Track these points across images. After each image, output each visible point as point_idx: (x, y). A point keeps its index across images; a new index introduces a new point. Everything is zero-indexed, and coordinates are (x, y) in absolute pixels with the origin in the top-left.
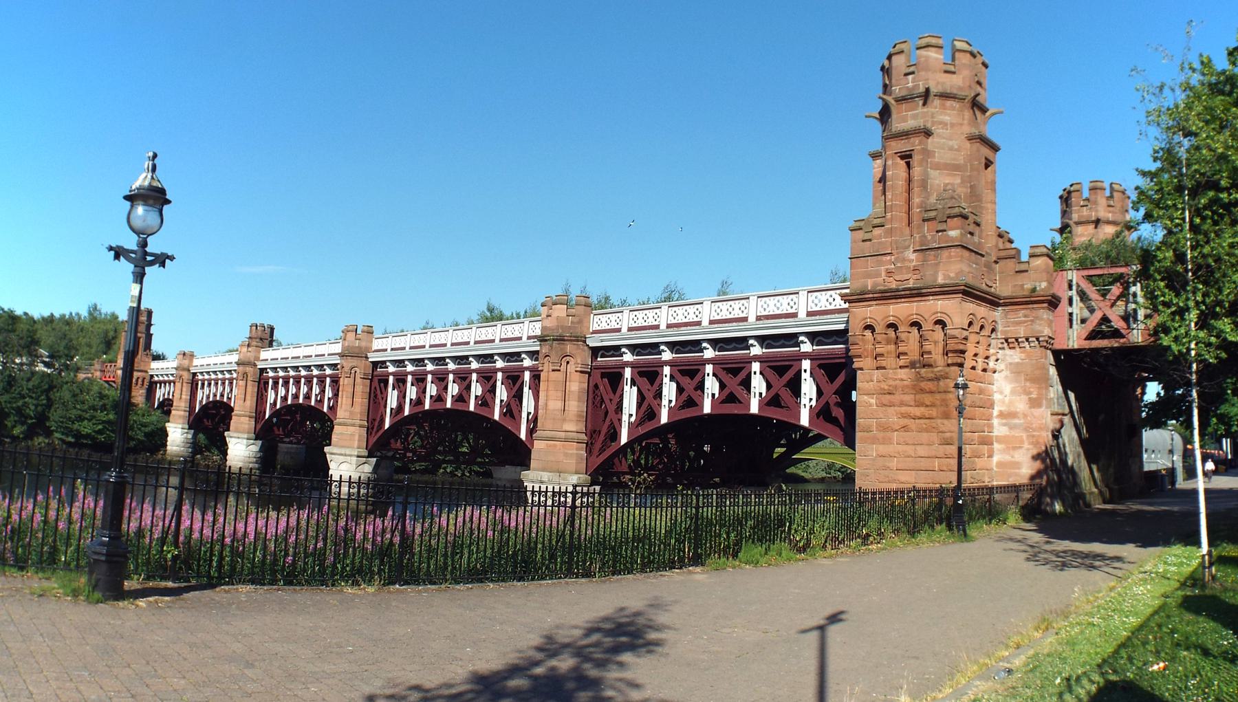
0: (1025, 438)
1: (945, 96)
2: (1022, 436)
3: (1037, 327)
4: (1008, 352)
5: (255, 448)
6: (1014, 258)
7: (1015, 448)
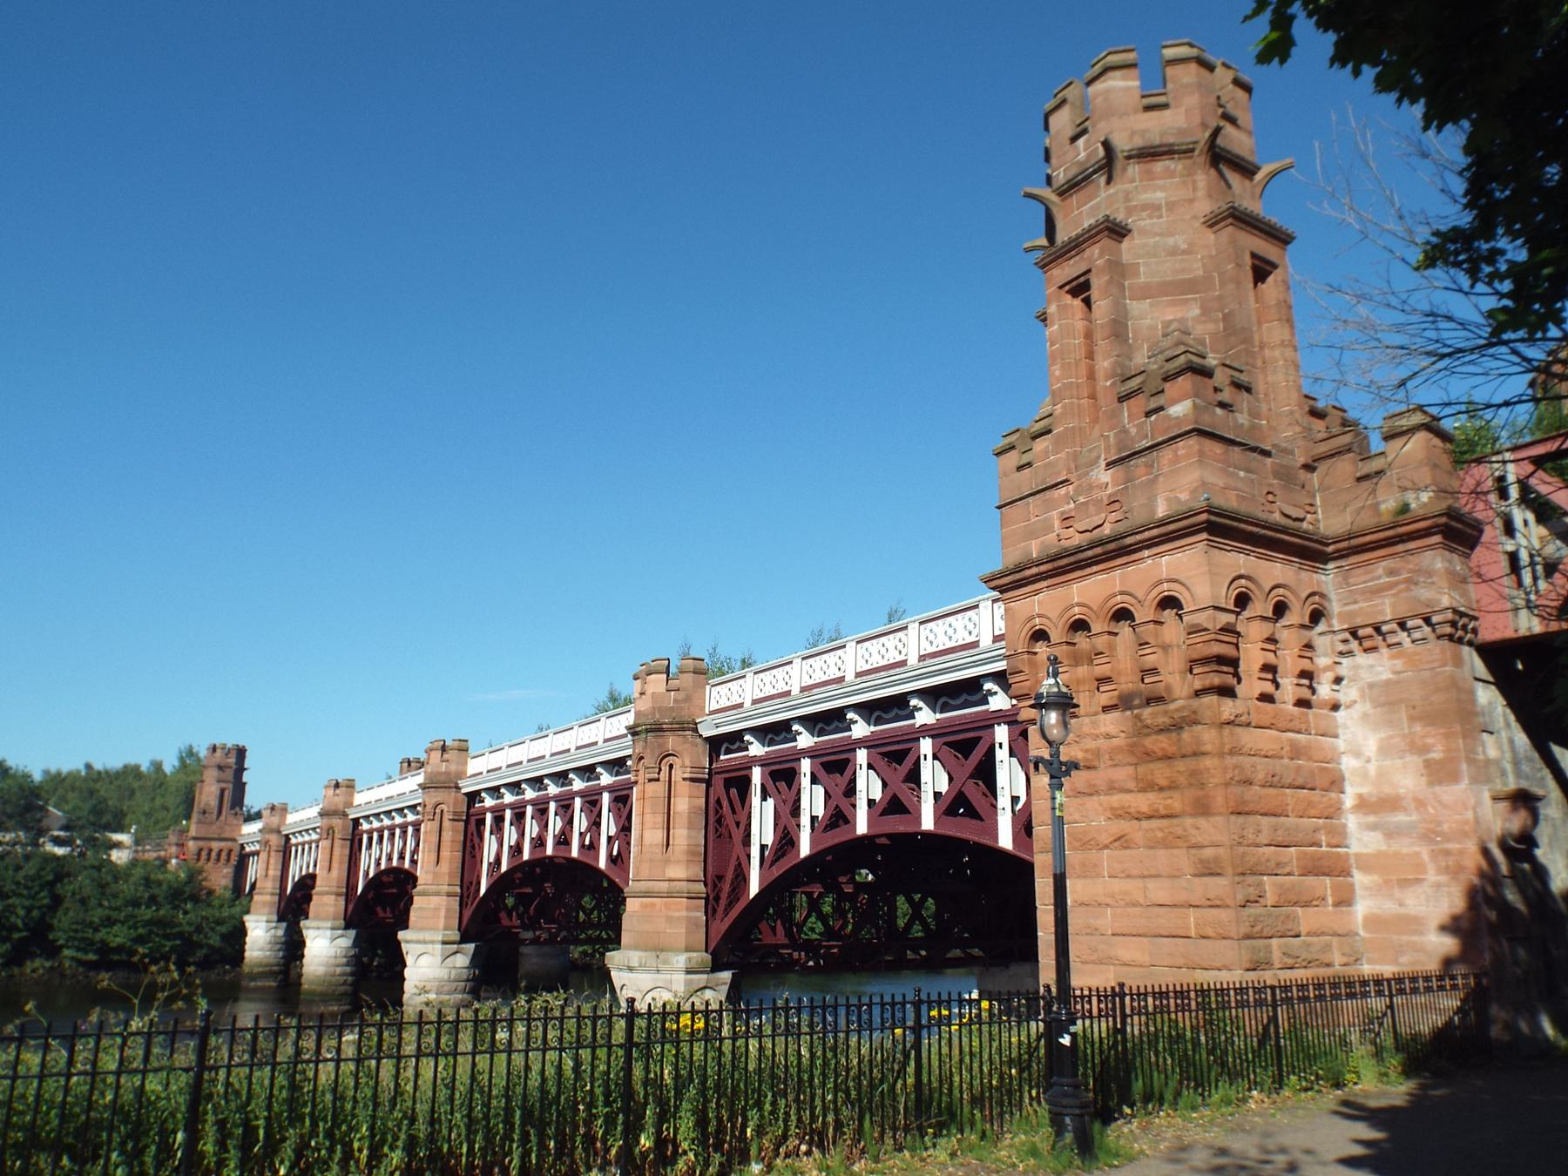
0: (1426, 857)
1: (1148, 154)
2: (1417, 854)
3: (1424, 593)
4: (1362, 659)
5: (345, 941)
6: (1349, 450)
7: (1404, 883)
